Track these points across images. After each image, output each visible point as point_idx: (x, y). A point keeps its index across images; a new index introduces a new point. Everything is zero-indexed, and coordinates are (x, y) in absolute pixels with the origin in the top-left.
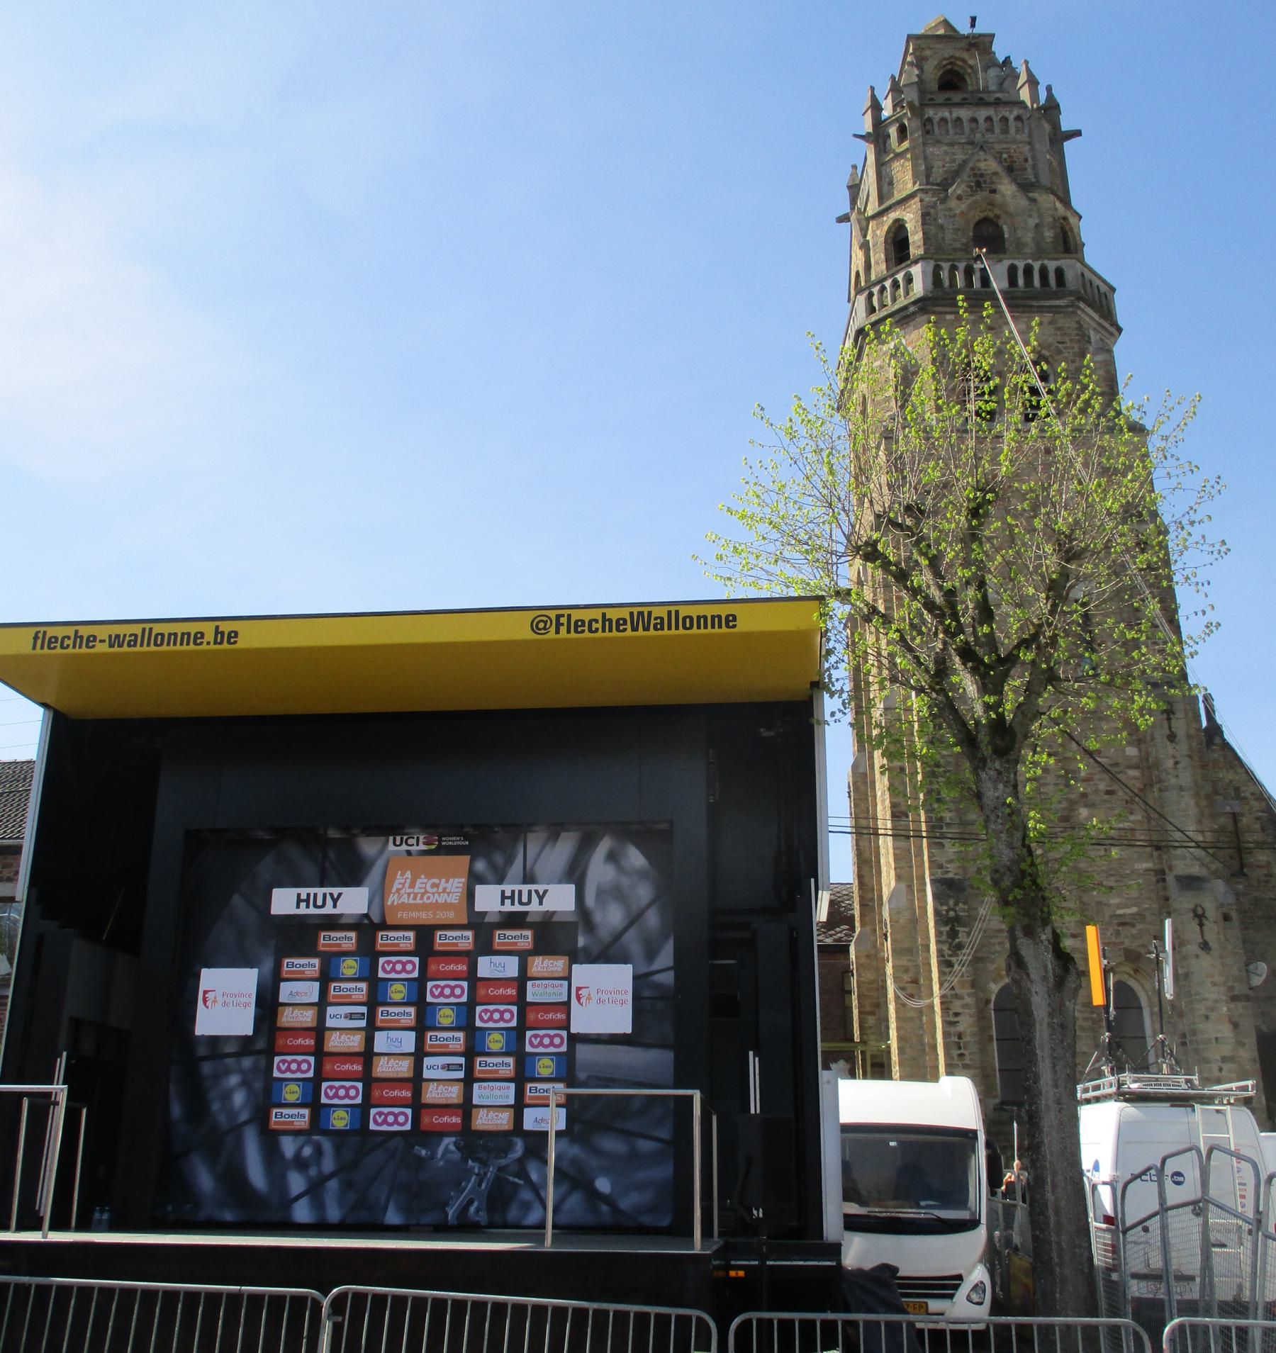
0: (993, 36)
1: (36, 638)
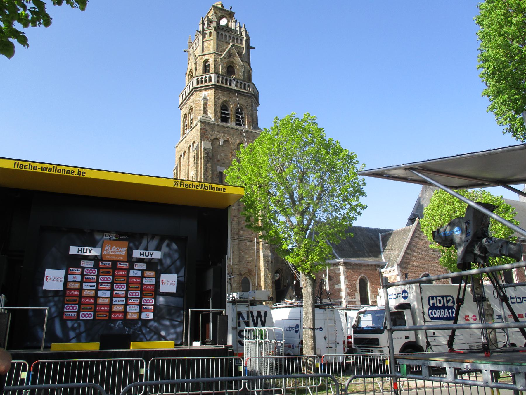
0: (235, 13)
1: (15, 164)
